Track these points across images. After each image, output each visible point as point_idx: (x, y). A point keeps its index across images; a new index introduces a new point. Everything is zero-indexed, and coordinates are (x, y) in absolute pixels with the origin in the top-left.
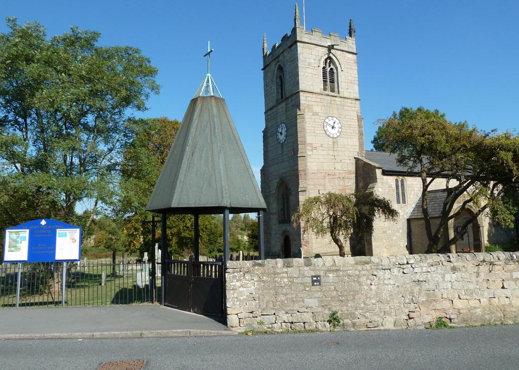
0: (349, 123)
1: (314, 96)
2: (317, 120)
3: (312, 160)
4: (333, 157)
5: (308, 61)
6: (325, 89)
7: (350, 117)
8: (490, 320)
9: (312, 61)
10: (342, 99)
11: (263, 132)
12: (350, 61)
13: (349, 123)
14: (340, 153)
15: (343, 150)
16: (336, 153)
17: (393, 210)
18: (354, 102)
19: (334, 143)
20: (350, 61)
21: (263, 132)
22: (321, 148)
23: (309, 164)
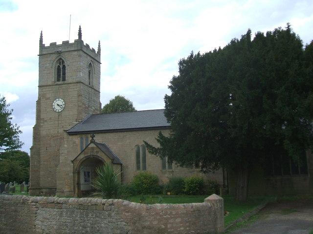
6: (58, 80)
9: (48, 65)
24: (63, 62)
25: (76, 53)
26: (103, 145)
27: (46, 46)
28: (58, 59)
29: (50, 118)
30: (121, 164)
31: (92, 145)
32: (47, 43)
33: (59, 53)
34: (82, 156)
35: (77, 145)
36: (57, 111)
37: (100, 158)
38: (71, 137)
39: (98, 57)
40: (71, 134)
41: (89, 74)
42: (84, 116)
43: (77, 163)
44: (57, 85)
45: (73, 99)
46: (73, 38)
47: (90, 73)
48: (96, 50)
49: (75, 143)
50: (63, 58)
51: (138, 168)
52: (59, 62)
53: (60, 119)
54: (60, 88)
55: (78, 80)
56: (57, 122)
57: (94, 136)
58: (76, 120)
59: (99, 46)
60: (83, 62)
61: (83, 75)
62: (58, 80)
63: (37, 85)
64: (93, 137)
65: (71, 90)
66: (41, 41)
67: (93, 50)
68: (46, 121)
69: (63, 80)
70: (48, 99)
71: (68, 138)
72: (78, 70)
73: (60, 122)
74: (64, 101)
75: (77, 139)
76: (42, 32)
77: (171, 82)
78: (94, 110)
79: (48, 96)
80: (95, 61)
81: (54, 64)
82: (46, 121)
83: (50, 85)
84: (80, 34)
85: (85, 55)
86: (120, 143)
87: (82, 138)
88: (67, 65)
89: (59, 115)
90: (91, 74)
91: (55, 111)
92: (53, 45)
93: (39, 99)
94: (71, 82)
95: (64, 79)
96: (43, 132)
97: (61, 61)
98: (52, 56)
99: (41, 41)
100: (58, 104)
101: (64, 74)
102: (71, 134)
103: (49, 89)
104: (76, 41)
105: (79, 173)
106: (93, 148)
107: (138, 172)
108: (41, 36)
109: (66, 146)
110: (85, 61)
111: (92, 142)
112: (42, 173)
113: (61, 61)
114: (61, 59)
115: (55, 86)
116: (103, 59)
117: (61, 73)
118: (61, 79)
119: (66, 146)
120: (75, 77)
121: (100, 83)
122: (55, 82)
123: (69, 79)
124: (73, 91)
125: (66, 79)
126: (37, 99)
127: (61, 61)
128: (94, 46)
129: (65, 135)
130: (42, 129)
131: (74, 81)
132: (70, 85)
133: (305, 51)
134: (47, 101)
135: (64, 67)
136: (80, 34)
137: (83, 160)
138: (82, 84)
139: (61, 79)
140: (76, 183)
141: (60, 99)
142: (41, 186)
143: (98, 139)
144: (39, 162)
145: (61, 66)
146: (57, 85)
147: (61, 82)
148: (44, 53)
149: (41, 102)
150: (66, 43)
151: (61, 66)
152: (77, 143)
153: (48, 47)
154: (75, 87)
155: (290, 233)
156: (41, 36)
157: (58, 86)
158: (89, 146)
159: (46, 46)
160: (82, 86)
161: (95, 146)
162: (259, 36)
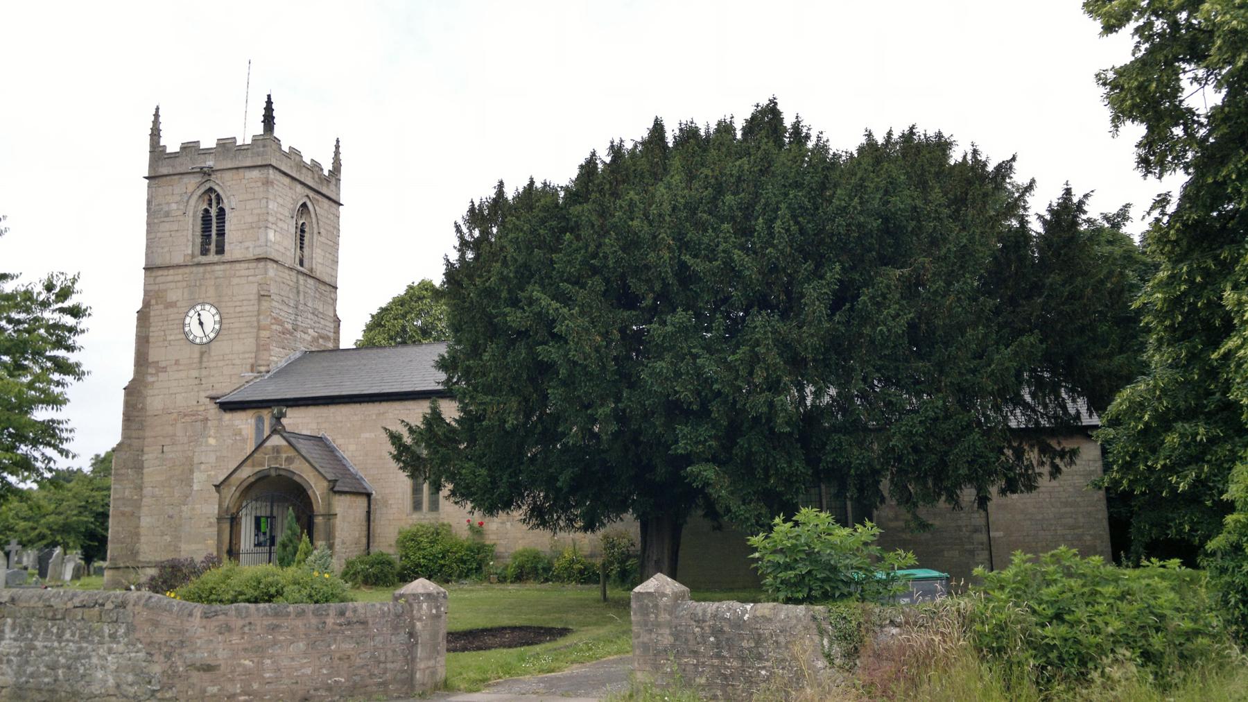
0: (238, 309)
1: (171, 272)
2: (172, 317)
3: (156, 392)
4: (197, 382)
5: (166, 208)
6: (205, 252)
7: (241, 298)
8: (1204, 678)
9: (174, 206)
10: (228, 266)
11: (767, 120)
12: (252, 185)
13: (238, 309)
14: (213, 372)
15: (220, 364)
16: (204, 373)
17: (1190, 110)
18: (254, 265)
19: (202, 354)
20: (252, 185)
21: (767, 120)
22: (175, 368)
23: (149, 400)
24: (219, 198)
25: (255, 174)
26: (319, 440)
27: (168, 151)
28: (203, 189)
29: (177, 362)
30: (369, 495)
31: (276, 440)
32: (171, 143)
33: (206, 173)
34: (246, 473)
36: (198, 341)
37: (296, 478)
38: (228, 417)
39: (332, 187)
40: (229, 407)
41: (302, 240)
42: (278, 358)
43: (231, 493)
44: (198, 264)
45: (244, 309)
46: (247, 130)
47: (303, 231)
48: (327, 167)
50: (216, 188)
51: (417, 506)
52: (206, 197)
53: (204, 365)
55: (259, 252)
57: (284, 415)
58: (252, 366)
59: (337, 153)
60: (279, 200)
61: (279, 240)
62: (205, 252)
63: (142, 263)
64: (278, 418)
66: (155, 133)
67: (316, 166)
68: (164, 369)
70: (172, 305)
71: (221, 419)
72: (261, 224)
74: (219, 312)
75: (244, 423)
76: (157, 109)
78: (315, 340)
79: (172, 296)
80: (318, 197)
81: (193, 202)
83: (179, 266)
84: (269, 120)
85: (287, 180)
86: (367, 435)
87: (260, 420)
88: (225, 202)
90: (307, 236)
91: (193, 342)
92: (190, 148)
93: (146, 304)
95: (220, 250)
96: (155, 402)
97: (213, 196)
98: (186, 179)
99: (155, 133)
100: (203, 322)
101: (221, 233)
102: (229, 407)
103: (177, 278)
104: (255, 139)
105: (234, 521)
106: (277, 449)
107: (415, 516)
108: (156, 122)
110: (282, 200)
111: (274, 431)
112: (145, 521)
113: (213, 196)
114: (211, 190)
115: (194, 269)
116: (347, 190)
118: (213, 247)
119: (212, 441)
121: (147, 255)
122: (193, 256)
123: (233, 249)
124: (244, 284)
125: (227, 247)
126: (139, 306)
127: (211, 195)
128: (317, 152)
129: (213, 409)
130: (151, 392)
131: (250, 256)
132: (238, 265)
134: (171, 310)
135: (221, 213)
136: (269, 120)
137: (245, 484)
138: (270, 265)
139: (213, 247)
140: (225, 547)
141: (207, 307)
142: (141, 558)
143: (296, 420)
144: (140, 488)
145: (214, 212)
146: (198, 264)
147: (212, 257)
148: (164, 171)
149: (152, 313)
150: (226, 146)
151: (214, 212)
152: (244, 433)
153: (174, 156)
154: (252, 272)
156: (156, 122)
157: (201, 269)
158: (268, 444)
159: (168, 151)
160: (272, 269)
161: (284, 443)
162: (689, 134)
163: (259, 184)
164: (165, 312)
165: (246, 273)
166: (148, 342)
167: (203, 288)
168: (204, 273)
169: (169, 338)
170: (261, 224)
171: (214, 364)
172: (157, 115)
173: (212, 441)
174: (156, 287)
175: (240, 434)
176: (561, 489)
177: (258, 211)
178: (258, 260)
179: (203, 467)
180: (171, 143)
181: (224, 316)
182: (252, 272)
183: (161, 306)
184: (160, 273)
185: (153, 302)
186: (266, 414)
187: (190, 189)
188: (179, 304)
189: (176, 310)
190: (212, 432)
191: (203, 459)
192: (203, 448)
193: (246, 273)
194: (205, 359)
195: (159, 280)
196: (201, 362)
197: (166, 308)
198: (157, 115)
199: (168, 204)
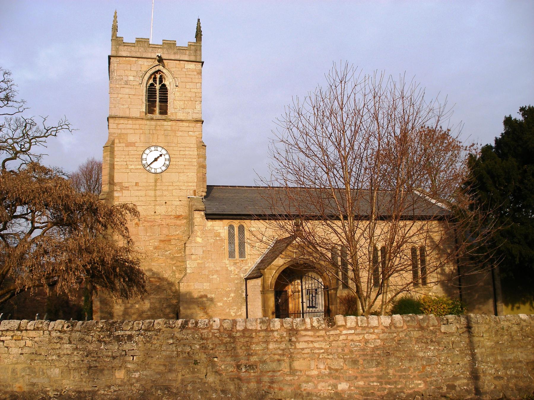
0: (182, 153)
1: (130, 122)
2: (132, 152)
9: (131, 78)
13: (182, 153)
14: (165, 193)
18: (193, 124)
22: (136, 188)
28: (154, 70)
35: (222, 240)
38: (210, 223)
45: (187, 153)
49: (218, 235)
53: (158, 188)
54: (158, 128)
56: (152, 193)
65: (180, 134)
68: (127, 188)
69: (161, 113)
70: (133, 144)
73: (158, 193)
76: (116, 13)
77: (81, 169)
79: (131, 139)
81: (146, 78)
82: (127, 188)
83: (137, 119)
89: (156, 181)
94: (182, 118)
95: (164, 111)
97: (158, 76)
99: (115, 29)
109: (199, 240)
113: (158, 76)
117: (158, 100)
120: (190, 111)
127: (157, 76)
131: (190, 118)
132: (181, 124)
133: (525, 119)
134: (131, 148)
136: (199, 35)
139: (157, 109)
145: (158, 86)
151: (158, 86)
152: (222, 235)
154: (192, 129)
155: (467, 398)
163: (195, 73)
164: (126, 149)
165: (187, 129)
166: (114, 168)
167: (156, 136)
168: (156, 126)
169: (130, 167)
170: (197, 99)
171: (165, 188)
172: (115, 17)
173: (199, 240)
174: (119, 131)
175: (219, 236)
176: (41, 298)
177: (195, 90)
178: (197, 121)
179: (193, 257)
180: (128, 35)
181: (172, 156)
182: (192, 129)
183: (124, 145)
184: (122, 121)
185: (117, 141)
186: (236, 223)
187: (144, 69)
188: (137, 145)
189: (135, 148)
190: (199, 234)
191: (193, 251)
192: (193, 245)
193: (187, 129)
194: (158, 184)
195: (120, 126)
196: (156, 186)
197: (127, 146)
198: (115, 17)
199: (127, 76)
